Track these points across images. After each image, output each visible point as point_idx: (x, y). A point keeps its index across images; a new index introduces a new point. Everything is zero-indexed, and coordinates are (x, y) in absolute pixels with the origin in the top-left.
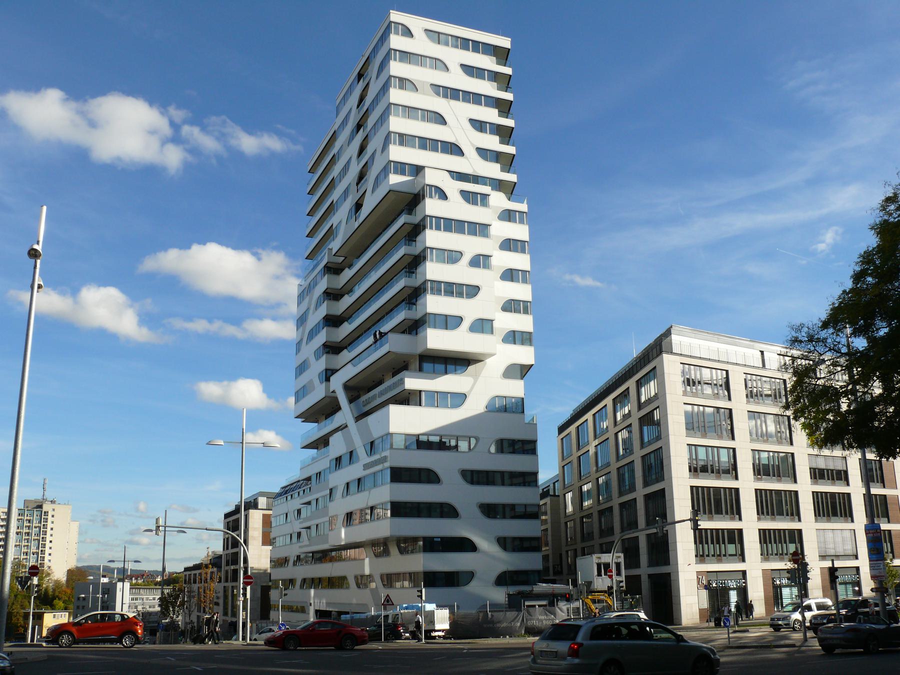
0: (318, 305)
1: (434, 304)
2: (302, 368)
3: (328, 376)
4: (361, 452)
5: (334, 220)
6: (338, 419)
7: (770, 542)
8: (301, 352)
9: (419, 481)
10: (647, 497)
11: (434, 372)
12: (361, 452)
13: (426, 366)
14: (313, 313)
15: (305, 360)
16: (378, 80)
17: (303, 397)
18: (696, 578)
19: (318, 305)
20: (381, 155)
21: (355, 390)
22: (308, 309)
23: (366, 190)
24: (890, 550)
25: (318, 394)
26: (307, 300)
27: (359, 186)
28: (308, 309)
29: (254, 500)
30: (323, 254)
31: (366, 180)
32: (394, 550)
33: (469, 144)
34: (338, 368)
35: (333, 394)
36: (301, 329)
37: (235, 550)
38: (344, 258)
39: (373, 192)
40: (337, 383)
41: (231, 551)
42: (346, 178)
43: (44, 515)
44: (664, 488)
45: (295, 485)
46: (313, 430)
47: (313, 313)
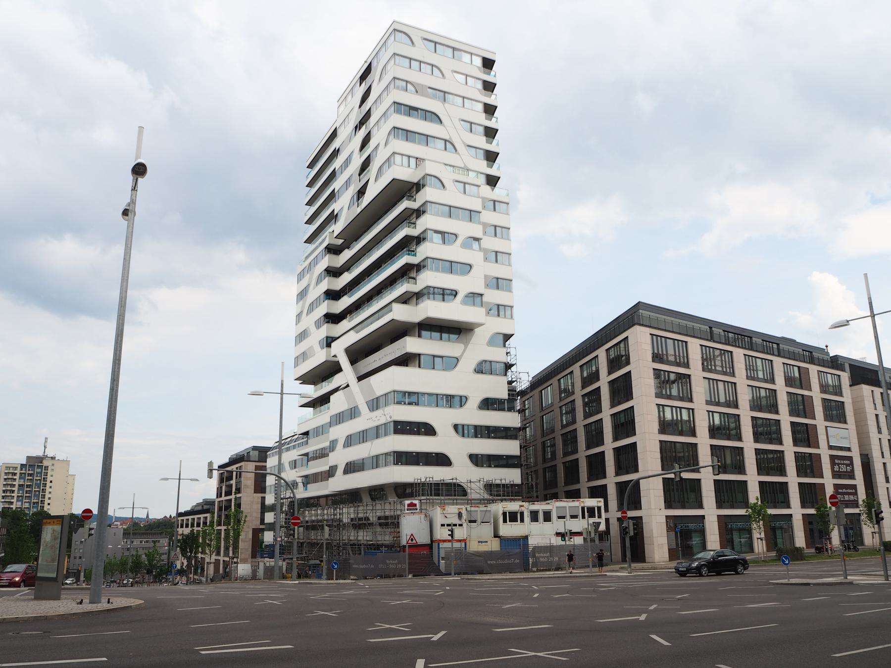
0: (319, 280)
1: (427, 279)
2: (302, 336)
3: (328, 342)
4: (364, 408)
5: (335, 206)
6: (337, 380)
7: (723, 492)
8: (300, 323)
9: (418, 433)
10: (617, 451)
11: (431, 338)
12: (364, 408)
13: (424, 333)
14: (314, 288)
15: (306, 329)
16: (381, 83)
17: (303, 361)
18: (665, 521)
19: (319, 280)
20: (384, 148)
21: (357, 354)
22: (308, 285)
23: (369, 180)
24: (814, 501)
25: (319, 357)
26: (307, 277)
27: (361, 176)
28: (308, 285)
29: (247, 453)
30: (323, 237)
31: (368, 171)
32: (366, 499)
33: (461, 142)
34: (337, 336)
35: (335, 359)
36: (301, 303)
37: (228, 498)
38: (343, 240)
39: (376, 180)
40: (339, 350)
41: (224, 498)
42: (347, 170)
43: (45, 470)
44: (636, 442)
45: (289, 439)
46: (312, 392)
47: (314, 288)
